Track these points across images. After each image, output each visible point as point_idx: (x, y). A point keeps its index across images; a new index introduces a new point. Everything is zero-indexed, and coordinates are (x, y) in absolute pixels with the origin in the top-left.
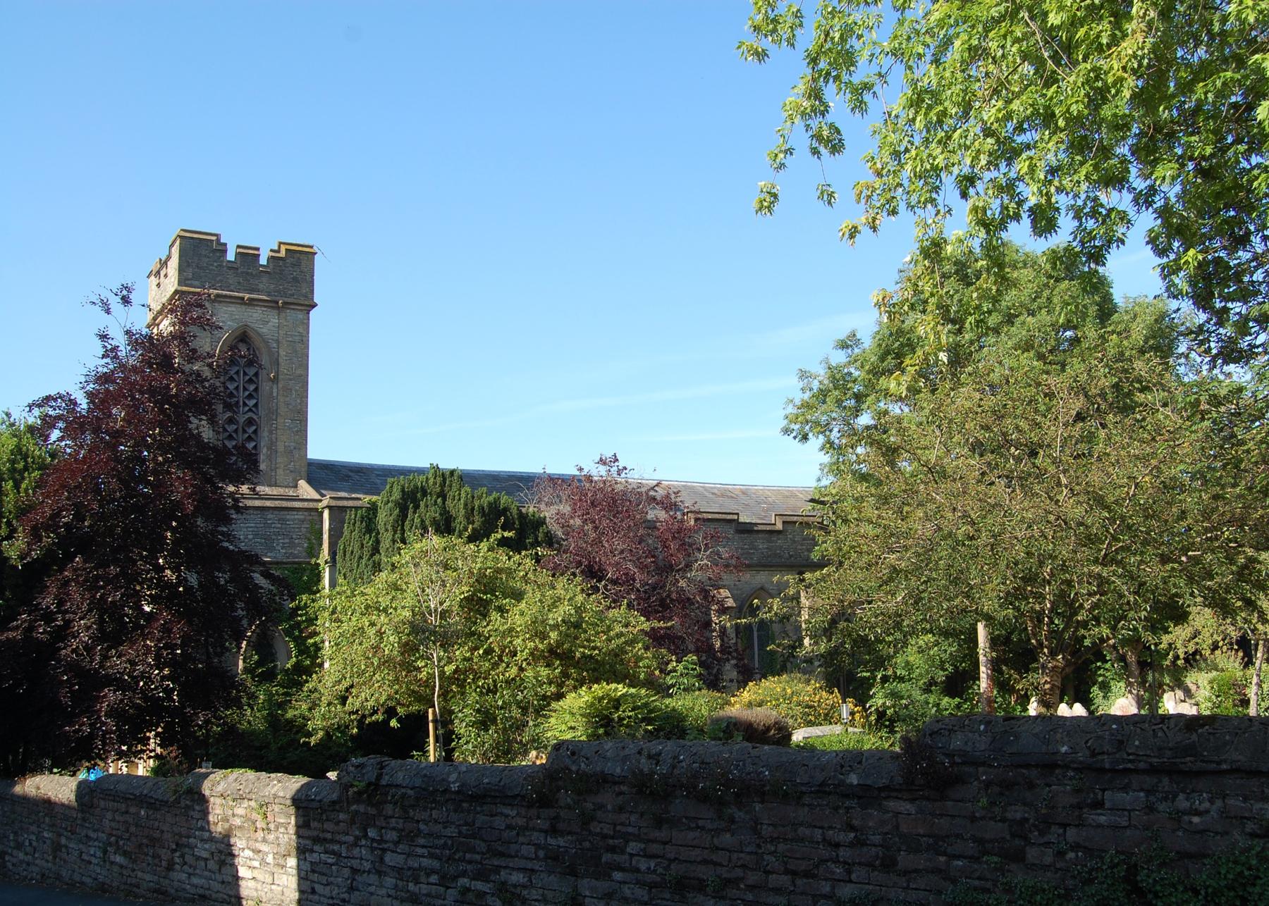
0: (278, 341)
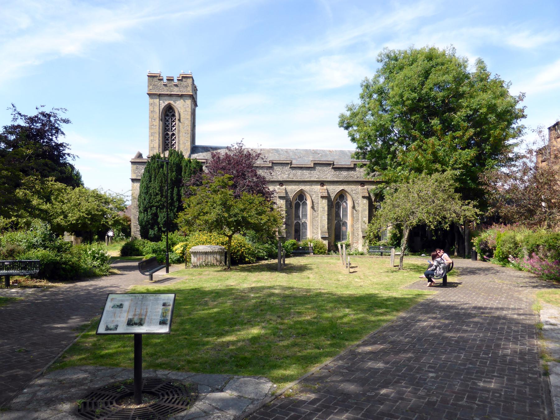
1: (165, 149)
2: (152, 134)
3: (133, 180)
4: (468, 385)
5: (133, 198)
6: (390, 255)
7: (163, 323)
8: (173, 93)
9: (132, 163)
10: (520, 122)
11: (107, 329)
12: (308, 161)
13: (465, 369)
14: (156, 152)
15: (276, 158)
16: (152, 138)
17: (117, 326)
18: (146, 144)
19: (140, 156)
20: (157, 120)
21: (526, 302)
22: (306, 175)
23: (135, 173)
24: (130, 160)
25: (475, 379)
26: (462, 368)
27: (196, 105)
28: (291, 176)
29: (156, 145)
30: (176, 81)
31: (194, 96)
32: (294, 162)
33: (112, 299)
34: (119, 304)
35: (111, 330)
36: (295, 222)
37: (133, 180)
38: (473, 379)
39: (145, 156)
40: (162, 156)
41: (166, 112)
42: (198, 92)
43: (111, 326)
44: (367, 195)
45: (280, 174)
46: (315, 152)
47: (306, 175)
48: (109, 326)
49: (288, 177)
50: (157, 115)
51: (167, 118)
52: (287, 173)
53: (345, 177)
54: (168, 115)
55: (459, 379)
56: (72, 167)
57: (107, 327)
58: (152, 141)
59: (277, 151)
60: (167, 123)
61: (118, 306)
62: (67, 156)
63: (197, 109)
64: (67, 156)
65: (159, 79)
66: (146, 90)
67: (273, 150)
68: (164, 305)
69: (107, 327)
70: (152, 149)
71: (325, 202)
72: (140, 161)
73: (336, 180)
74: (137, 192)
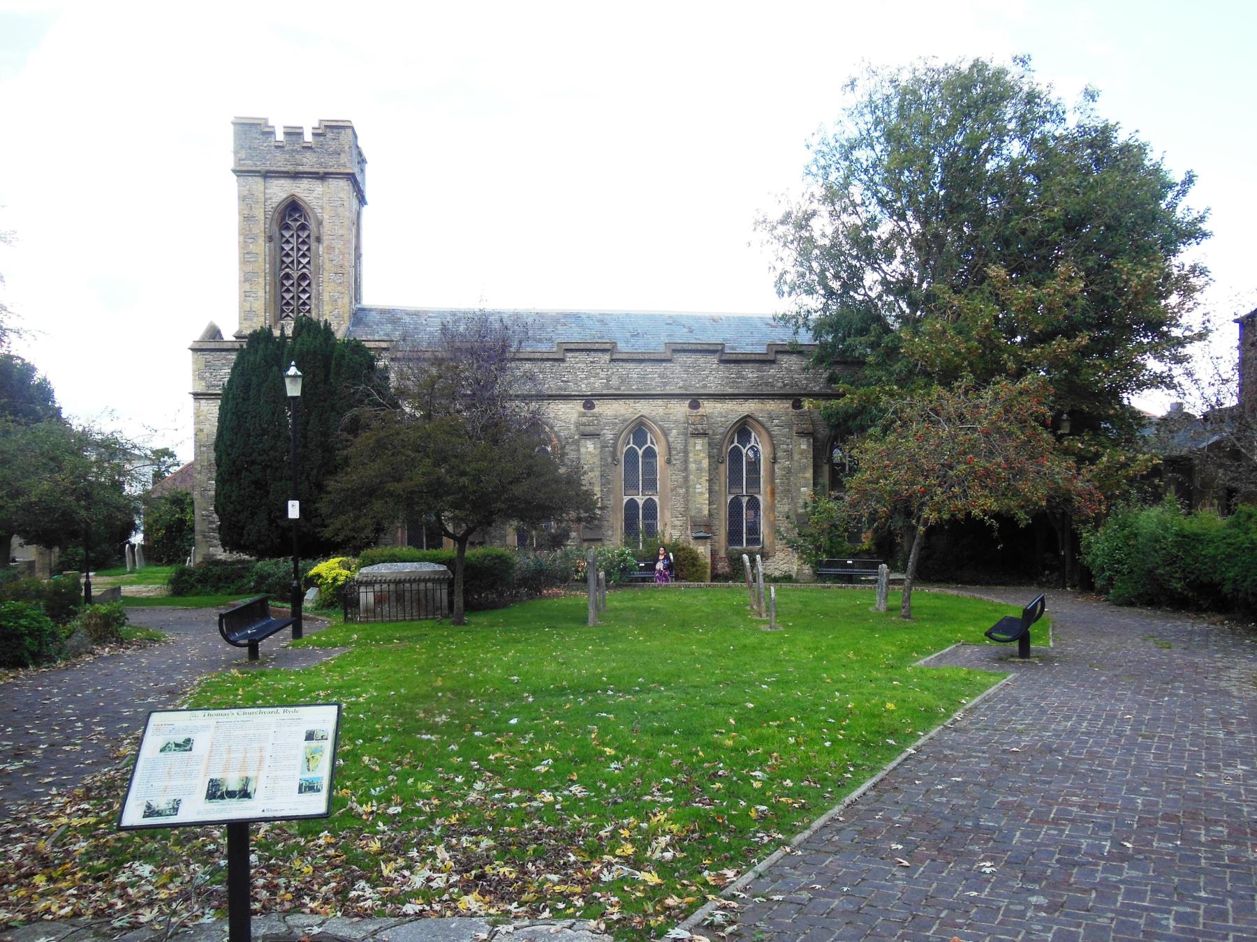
0: (322, 208)
1: (281, 315)
2: (247, 278)
3: (197, 396)
4: (1136, 926)
5: (199, 445)
6: (876, 581)
7: (308, 788)
8: (301, 169)
9: (194, 350)
10: (1187, 256)
11: (150, 812)
12: (657, 345)
13: (1122, 882)
14: (258, 323)
15: (574, 335)
16: (247, 287)
17: (178, 802)
18: (225, 299)
19: (214, 333)
20: (261, 241)
21: (1240, 698)
22: (653, 376)
23: (202, 378)
24: (190, 344)
25: (1153, 909)
26: (1114, 878)
27: (362, 200)
28: (615, 382)
29: (259, 305)
30: (308, 137)
31: (359, 178)
32: (621, 346)
33: (158, 728)
34: (180, 741)
35: (159, 814)
36: (626, 499)
37: (197, 396)
38: (1146, 909)
39: (228, 335)
40: (277, 333)
41: (283, 218)
42: (368, 168)
43: (161, 803)
44: (811, 429)
45: (585, 375)
46: (673, 322)
47: (653, 376)
48: (154, 804)
49: (607, 386)
50: (259, 228)
51: (287, 234)
52: (602, 375)
53: (753, 385)
54: (288, 227)
55: (1112, 911)
56: (29, 370)
57: (149, 807)
58: (245, 295)
59: (577, 317)
60: (287, 248)
61: (177, 745)
62: (13, 336)
63: (365, 209)
64: (13, 336)
65: (264, 133)
66: (230, 162)
67: (566, 316)
68: (310, 736)
69: (149, 807)
70: (246, 315)
71: (699, 444)
72: (217, 346)
73: (730, 391)
74: (212, 427)
